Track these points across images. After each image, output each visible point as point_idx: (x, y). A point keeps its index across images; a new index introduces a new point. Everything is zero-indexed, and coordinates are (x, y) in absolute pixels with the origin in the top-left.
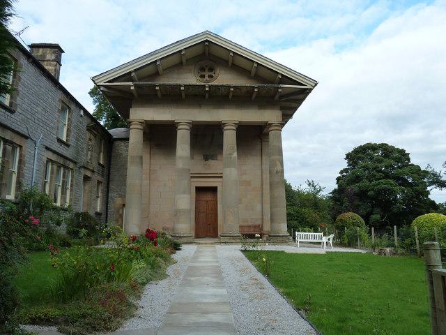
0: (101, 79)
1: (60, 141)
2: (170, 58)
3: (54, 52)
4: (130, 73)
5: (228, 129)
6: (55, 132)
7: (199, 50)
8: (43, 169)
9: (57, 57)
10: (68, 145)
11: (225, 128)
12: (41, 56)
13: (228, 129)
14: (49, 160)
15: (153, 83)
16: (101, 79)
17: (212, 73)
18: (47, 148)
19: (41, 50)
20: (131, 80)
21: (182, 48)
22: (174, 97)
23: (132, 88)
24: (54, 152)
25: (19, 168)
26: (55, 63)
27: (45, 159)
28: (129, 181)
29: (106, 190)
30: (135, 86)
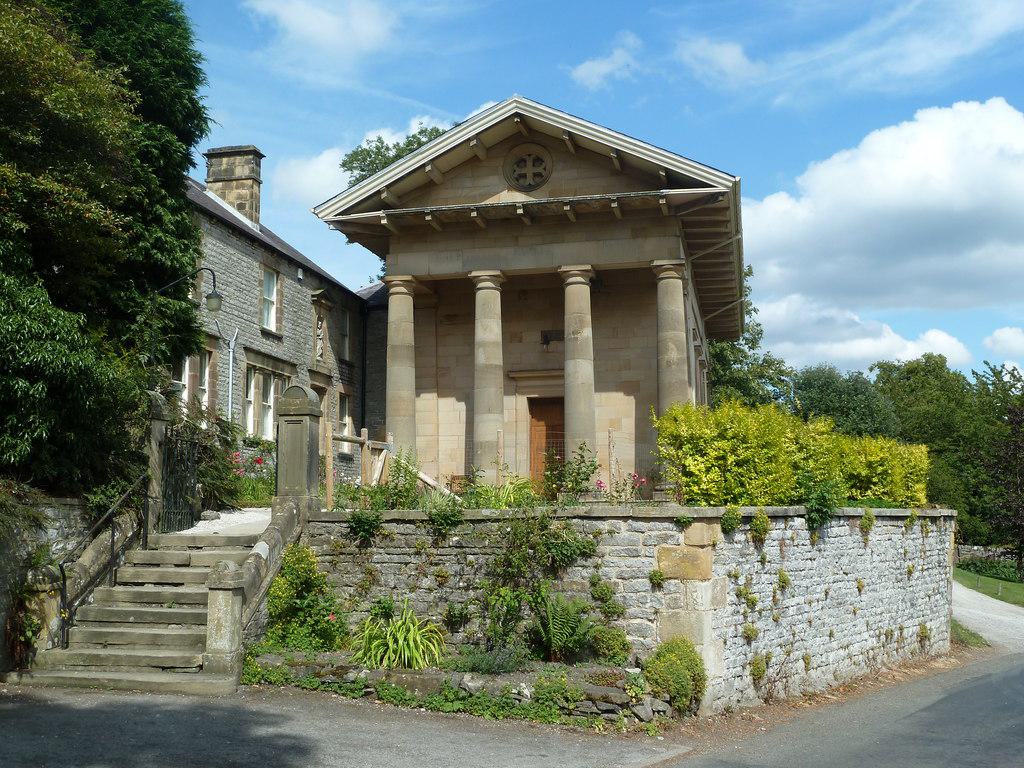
0: (327, 211)
1: (266, 334)
2: (491, 130)
3: (248, 162)
4: (379, 192)
5: (398, 293)
6: (256, 320)
7: (509, 130)
8: (242, 382)
9: (253, 170)
10: (278, 338)
11: (480, 285)
12: (226, 170)
13: (398, 293)
14: (251, 369)
15: (419, 209)
16: (327, 211)
17: (540, 170)
18: (247, 349)
19: (225, 160)
20: (384, 206)
21: (426, 161)
22: (462, 227)
23: (384, 222)
24: (258, 353)
25: (213, 385)
26: (250, 182)
27: (243, 366)
28: (391, 392)
29: (359, 410)
30: (388, 216)
